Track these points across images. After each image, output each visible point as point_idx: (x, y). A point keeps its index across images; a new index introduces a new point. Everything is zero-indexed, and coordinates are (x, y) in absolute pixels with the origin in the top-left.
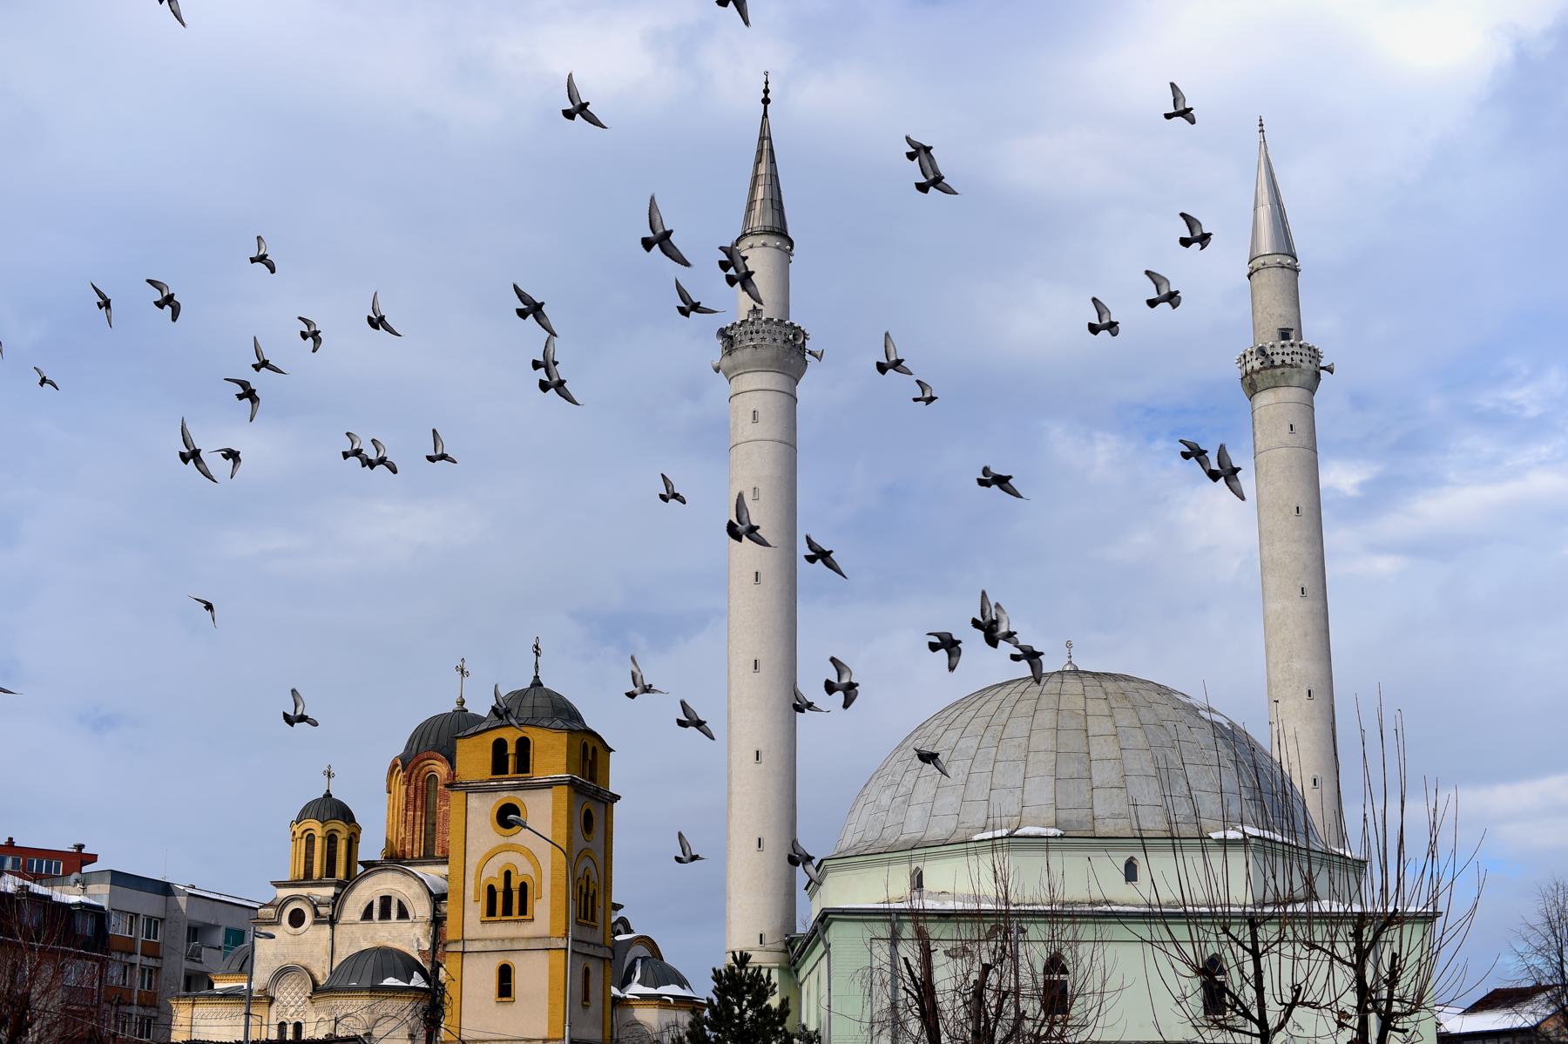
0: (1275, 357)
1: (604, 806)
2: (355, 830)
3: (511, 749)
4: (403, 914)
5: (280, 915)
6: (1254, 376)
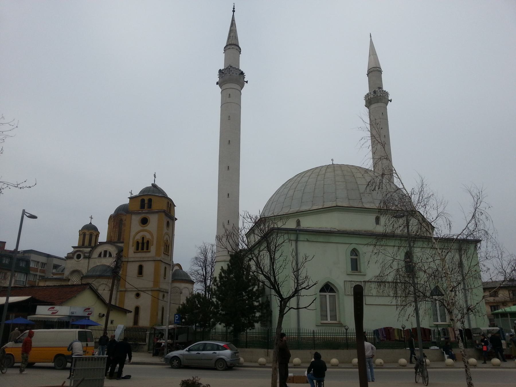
0: (378, 94)
1: (172, 221)
2: (98, 233)
3: (146, 202)
4: (110, 255)
5: (74, 255)
6: (371, 99)
